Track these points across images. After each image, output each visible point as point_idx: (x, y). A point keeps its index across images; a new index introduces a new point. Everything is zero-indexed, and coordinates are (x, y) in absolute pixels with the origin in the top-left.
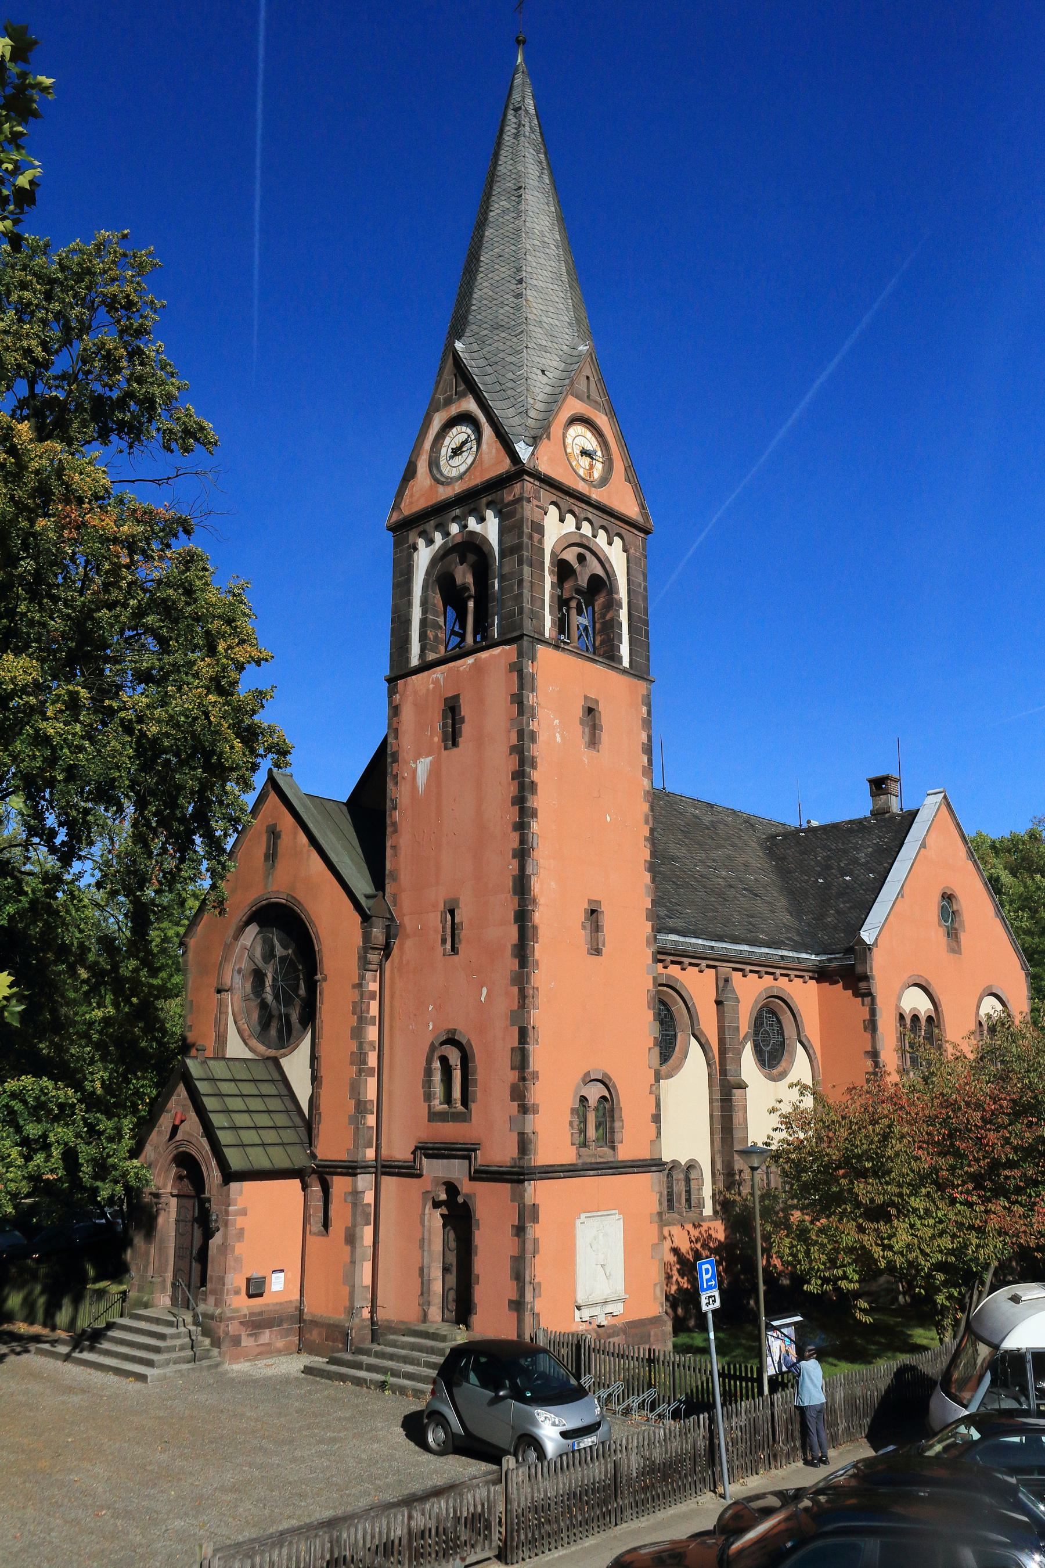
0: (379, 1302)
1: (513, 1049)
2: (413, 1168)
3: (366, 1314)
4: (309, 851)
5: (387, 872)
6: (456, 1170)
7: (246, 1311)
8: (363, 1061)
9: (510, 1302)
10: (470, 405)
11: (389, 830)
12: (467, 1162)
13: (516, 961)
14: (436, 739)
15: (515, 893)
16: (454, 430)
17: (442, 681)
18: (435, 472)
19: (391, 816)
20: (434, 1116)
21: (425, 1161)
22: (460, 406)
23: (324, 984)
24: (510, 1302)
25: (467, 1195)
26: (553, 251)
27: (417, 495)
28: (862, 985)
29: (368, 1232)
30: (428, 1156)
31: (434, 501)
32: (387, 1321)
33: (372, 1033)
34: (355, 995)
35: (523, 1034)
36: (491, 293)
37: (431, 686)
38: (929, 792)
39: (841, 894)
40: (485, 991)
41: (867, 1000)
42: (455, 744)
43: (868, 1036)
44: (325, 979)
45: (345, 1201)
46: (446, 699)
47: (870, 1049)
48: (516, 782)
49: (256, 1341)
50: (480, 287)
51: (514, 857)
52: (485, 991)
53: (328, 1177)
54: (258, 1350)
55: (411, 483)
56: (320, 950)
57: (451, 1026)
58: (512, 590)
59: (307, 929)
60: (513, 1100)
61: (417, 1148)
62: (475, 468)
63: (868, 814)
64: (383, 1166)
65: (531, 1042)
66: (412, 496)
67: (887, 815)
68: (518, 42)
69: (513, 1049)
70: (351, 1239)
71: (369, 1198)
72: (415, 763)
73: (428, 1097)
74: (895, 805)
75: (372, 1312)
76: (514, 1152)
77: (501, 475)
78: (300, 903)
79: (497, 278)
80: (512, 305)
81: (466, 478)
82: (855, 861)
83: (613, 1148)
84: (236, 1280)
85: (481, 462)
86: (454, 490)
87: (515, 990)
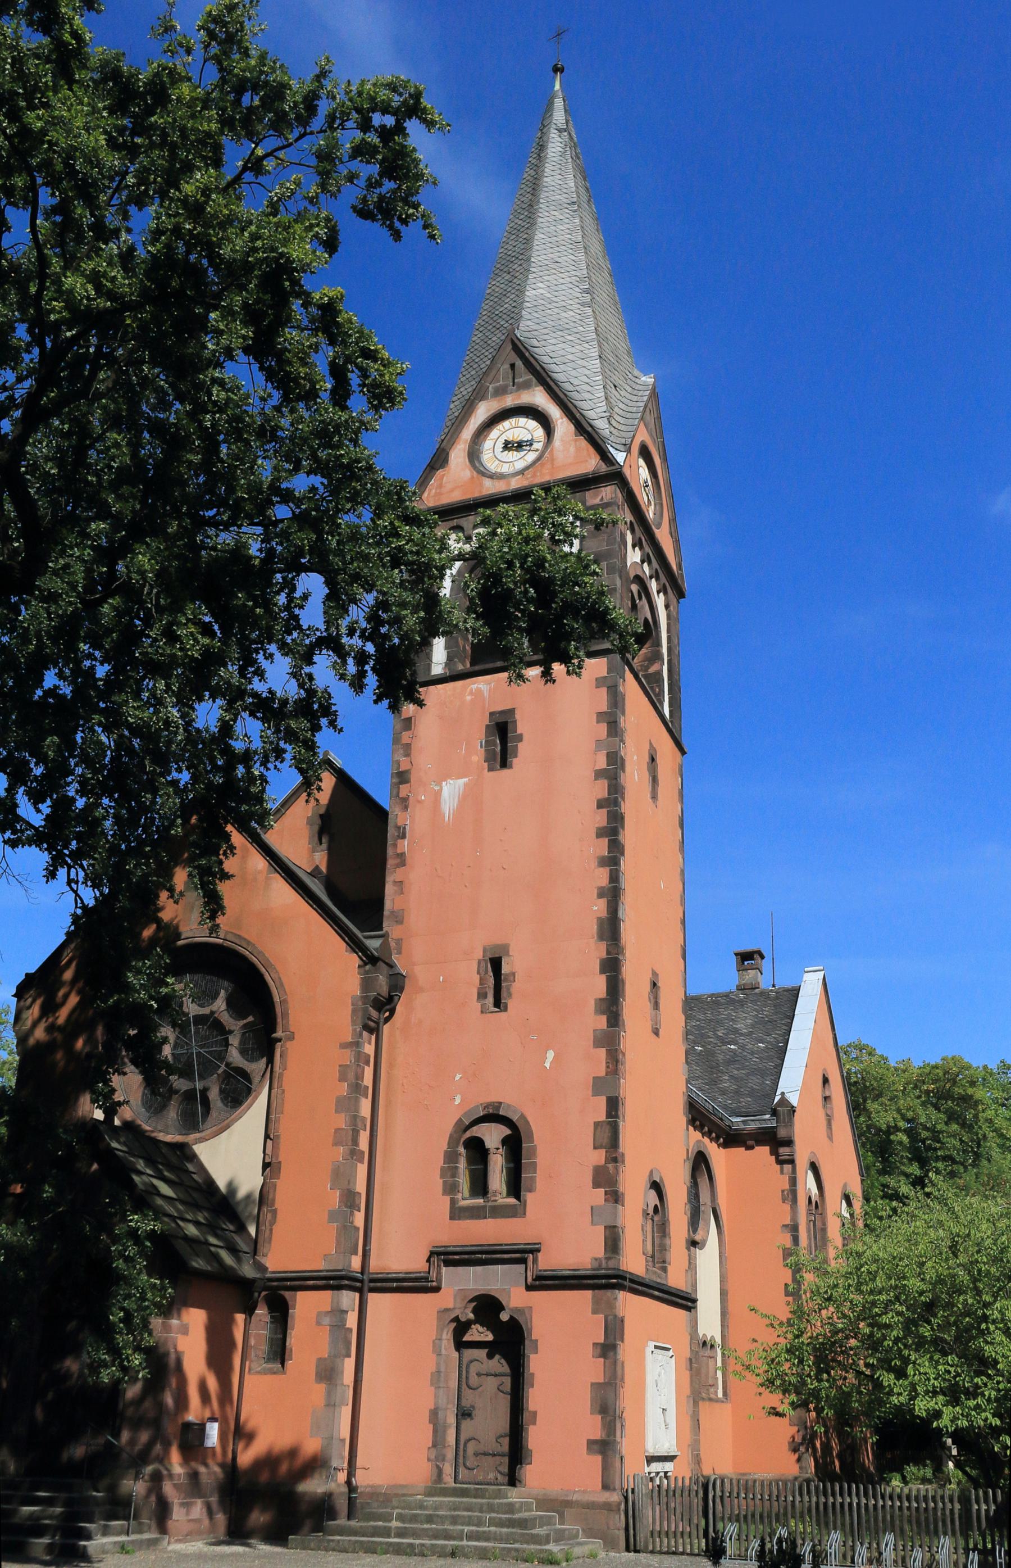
0: (360, 1462)
1: (597, 1125)
2: (426, 1279)
3: (342, 1477)
4: (267, 879)
5: (386, 913)
8: (355, 1142)
9: (591, 1443)
10: (539, 398)
11: (391, 863)
12: (523, 1266)
13: (604, 1019)
14: (475, 758)
15: (601, 937)
17: (486, 694)
18: (477, 465)
19: (395, 845)
20: (457, 1213)
21: (444, 1269)
22: (519, 397)
23: (289, 1044)
24: (591, 1443)
25: (520, 1311)
26: (606, 275)
27: (449, 486)
28: (783, 1150)
29: (349, 1365)
30: (448, 1263)
31: (476, 495)
32: (372, 1486)
33: (365, 1107)
34: (348, 1057)
35: (614, 1105)
36: (548, 295)
37: (469, 698)
38: (806, 969)
39: (729, 1062)
40: (550, 1055)
41: (787, 1167)
42: (504, 764)
43: (787, 1207)
44: (291, 1037)
45: (318, 1323)
46: (492, 714)
47: (788, 1222)
48: (604, 811)
49: (188, 1513)
50: (533, 286)
51: (600, 895)
52: (550, 1055)
53: (287, 1294)
54: (192, 1526)
55: (440, 472)
56: (284, 1002)
59: (261, 976)
60: (596, 1185)
61: (432, 1253)
62: (543, 465)
63: (734, 989)
64: (372, 1281)
65: (621, 1117)
66: (440, 486)
67: (757, 991)
68: (556, 69)
69: (597, 1125)
70: (327, 1373)
71: (352, 1321)
72: (439, 784)
73: (450, 1189)
74: (765, 982)
75: (351, 1474)
76: (600, 1252)
77: (586, 475)
78: (248, 942)
79: (555, 282)
80: (578, 311)
81: (529, 474)
82: (736, 1031)
83: (664, 1270)
85: (552, 460)
86: (509, 484)
87: (602, 1053)
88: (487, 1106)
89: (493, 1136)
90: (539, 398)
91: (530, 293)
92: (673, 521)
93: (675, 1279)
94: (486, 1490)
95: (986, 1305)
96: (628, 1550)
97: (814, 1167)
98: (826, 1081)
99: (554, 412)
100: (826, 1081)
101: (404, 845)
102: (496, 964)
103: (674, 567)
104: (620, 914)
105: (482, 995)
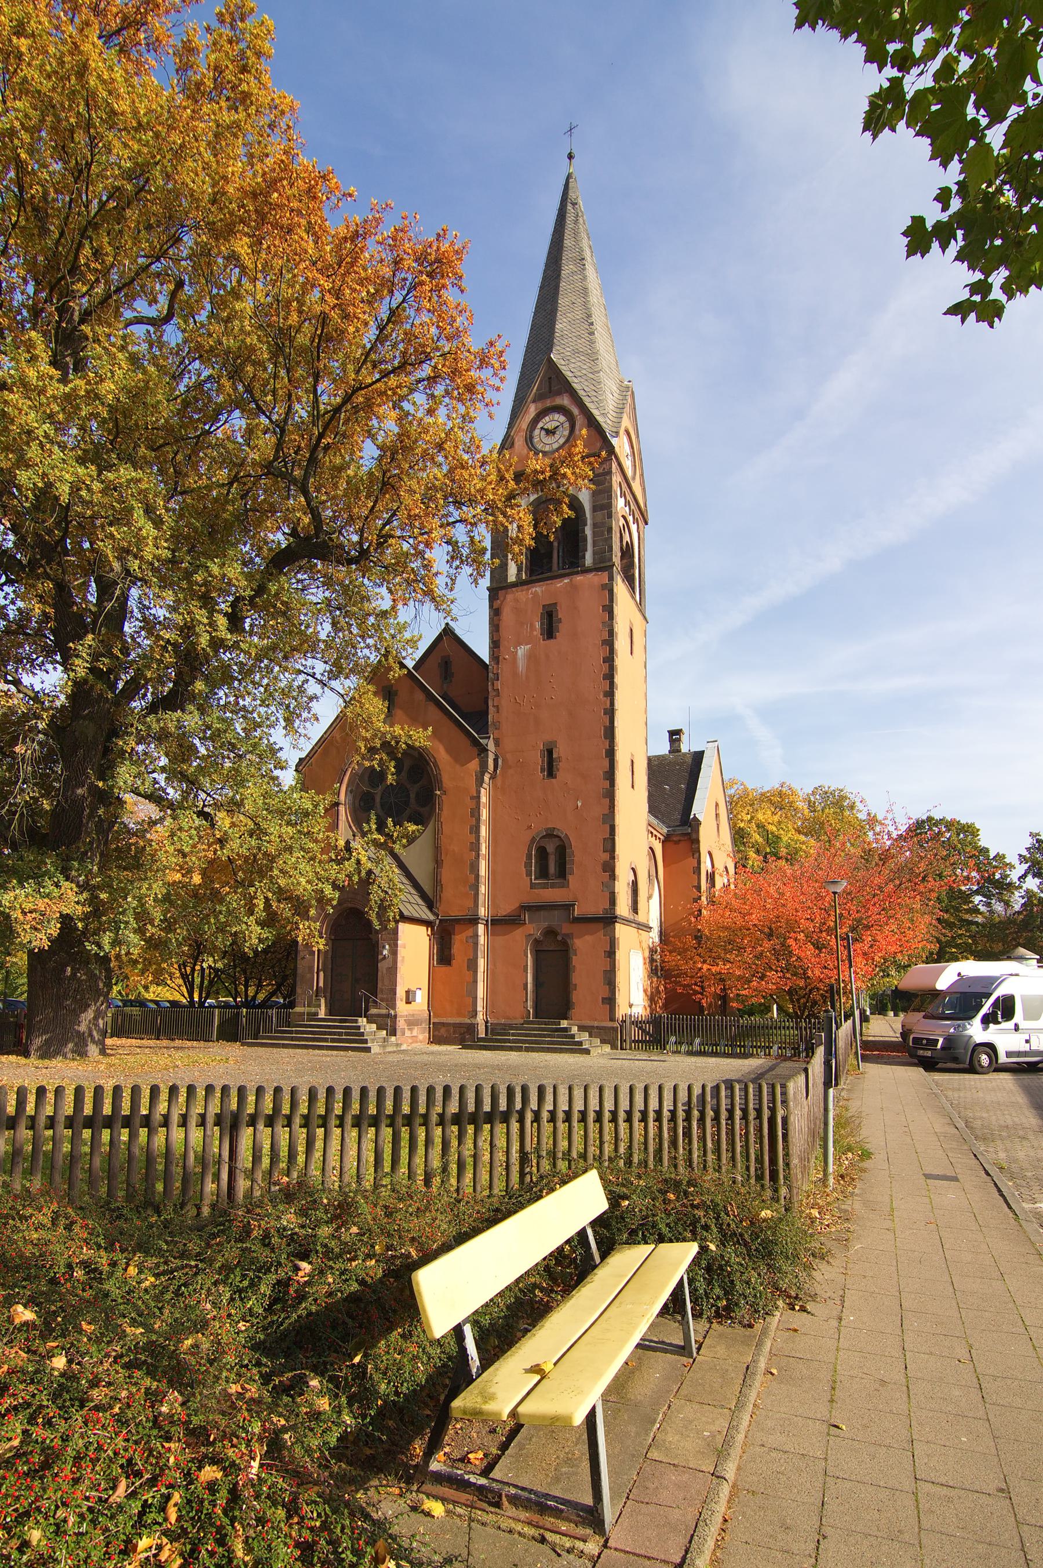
1: (604, 839)
6: (554, 919)
7: (406, 1013)
10: (565, 401)
16: (556, 416)
57: (550, 826)
58: (603, 535)
69: (604, 839)
73: (529, 874)
76: (607, 907)
84: (400, 992)
88: (547, 830)
89: (551, 848)
90: (565, 401)
91: (558, 326)
92: (642, 475)
93: (641, 918)
94: (838, 1117)
95: (29, 65)
96: (622, 1049)
97: (710, 854)
98: (717, 805)
99: (575, 411)
100: (717, 805)
101: (498, 685)
102: (550, 752)
103: (642, 505)
104: (616, 724)
105: (542, 770)
